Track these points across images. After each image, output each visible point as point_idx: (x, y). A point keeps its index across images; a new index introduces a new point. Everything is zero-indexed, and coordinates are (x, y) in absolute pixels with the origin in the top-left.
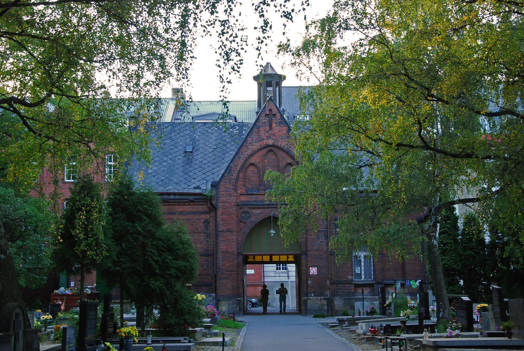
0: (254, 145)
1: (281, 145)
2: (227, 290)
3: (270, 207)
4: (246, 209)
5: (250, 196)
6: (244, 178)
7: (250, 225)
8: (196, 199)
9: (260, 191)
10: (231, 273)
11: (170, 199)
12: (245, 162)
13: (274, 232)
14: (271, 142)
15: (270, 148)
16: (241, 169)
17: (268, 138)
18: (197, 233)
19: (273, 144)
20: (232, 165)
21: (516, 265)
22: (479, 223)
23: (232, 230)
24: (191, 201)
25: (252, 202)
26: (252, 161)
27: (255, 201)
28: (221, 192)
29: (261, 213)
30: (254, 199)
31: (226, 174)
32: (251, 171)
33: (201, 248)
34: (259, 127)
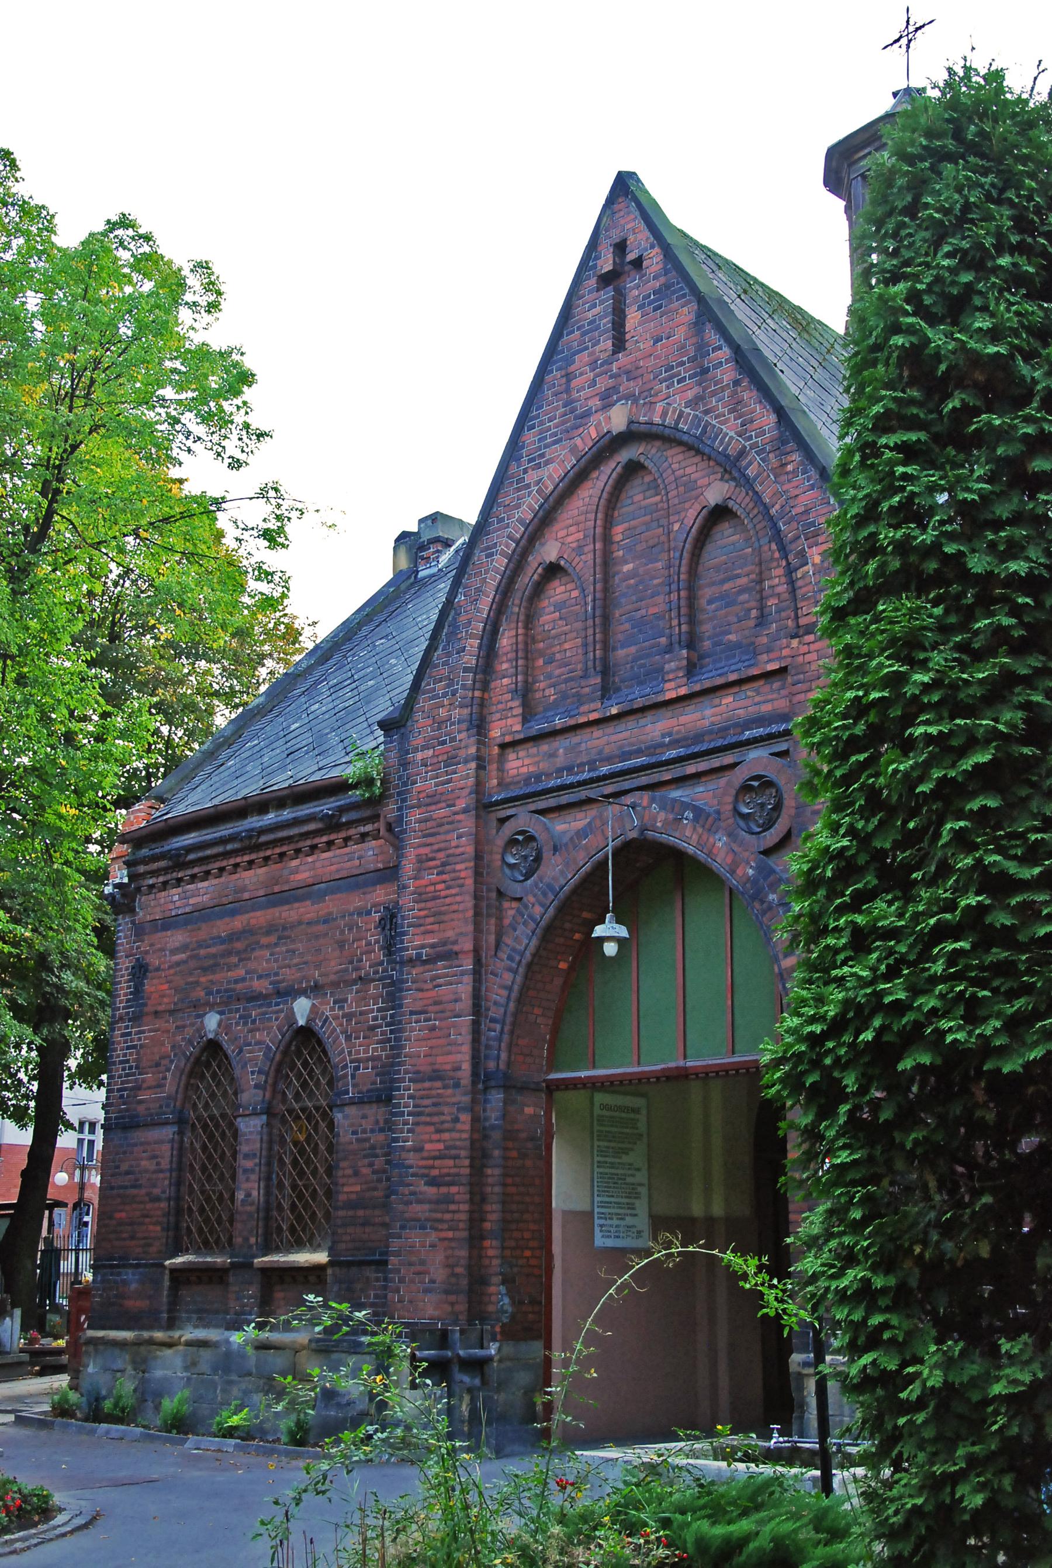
0: (547, 463)
1: (664, 414)
2: (426, 1291)
3: (626, 785)
4: (523, 819)
5: (545, 747)
6: (527, 651)
7: (538, 910)
8: (342, 810)
9: (584, 708)
10: (444, 1190)
11: (262, 831)
12: (518, 562)
13: (622, 932)
14: (618, 419)
15: (625, 455)
16: (500, 608)
17: (608, 399)
18: (354, 982)
19: (631, 422)
20: (460, 598)
21: (943, 1254)
22: (1033, 222)
23: (456, 948)
24: (332, 824)
25: (559, 771)
26: (550, 551)
27: (570, 769)
28: (416, 750)
29: (582, 834)
30: (560, 761)
31: (439, 652)
32: (558, 607)
33: (368, 1059)
34: (569, 360)
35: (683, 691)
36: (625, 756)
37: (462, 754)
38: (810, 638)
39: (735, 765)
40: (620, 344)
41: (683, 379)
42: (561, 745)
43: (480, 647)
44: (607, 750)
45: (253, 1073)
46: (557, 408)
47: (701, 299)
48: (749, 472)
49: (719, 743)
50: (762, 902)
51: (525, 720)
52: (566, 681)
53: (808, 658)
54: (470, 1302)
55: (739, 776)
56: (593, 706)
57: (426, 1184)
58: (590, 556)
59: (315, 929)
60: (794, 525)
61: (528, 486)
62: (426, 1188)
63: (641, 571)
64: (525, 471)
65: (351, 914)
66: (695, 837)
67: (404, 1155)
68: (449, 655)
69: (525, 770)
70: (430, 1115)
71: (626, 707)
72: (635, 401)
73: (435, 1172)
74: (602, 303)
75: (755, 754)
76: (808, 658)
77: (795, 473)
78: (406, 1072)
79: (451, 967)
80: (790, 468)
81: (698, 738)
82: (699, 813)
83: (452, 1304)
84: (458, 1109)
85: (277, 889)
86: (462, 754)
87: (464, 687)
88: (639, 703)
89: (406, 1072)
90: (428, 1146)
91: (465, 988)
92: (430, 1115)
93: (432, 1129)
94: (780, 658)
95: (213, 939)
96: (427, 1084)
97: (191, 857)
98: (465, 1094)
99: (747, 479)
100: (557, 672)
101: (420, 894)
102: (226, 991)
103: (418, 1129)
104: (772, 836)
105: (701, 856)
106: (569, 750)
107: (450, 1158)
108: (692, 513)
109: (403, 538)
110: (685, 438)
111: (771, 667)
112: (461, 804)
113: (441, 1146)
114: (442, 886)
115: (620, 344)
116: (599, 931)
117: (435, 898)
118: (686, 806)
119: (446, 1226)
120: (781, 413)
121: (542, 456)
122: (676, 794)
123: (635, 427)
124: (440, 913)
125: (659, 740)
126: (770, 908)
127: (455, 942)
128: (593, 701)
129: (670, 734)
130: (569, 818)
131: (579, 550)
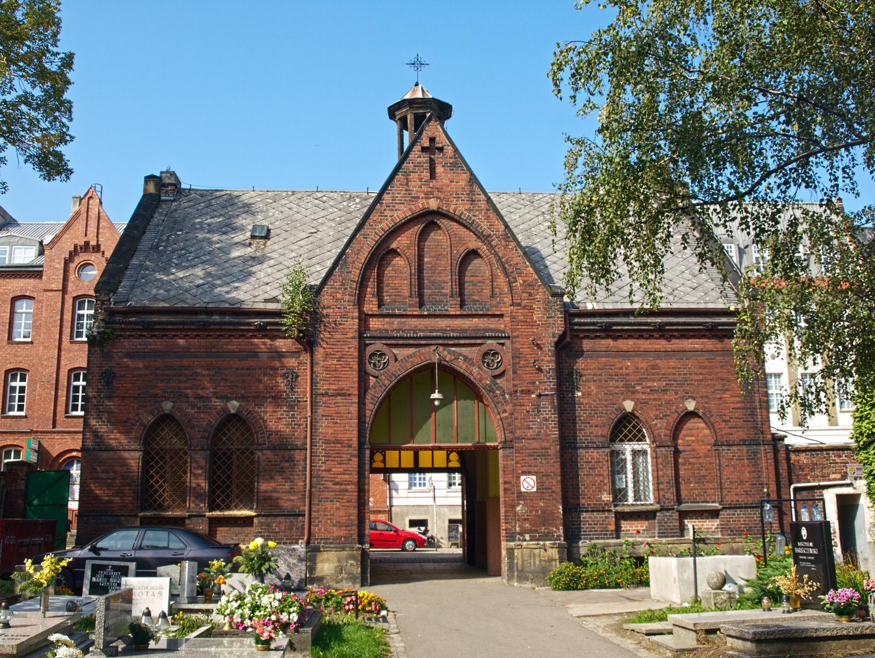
0: (396, 210)
7: (387, 382)
15: (430, 218)
17: (428, 196)
19: (439, 208)
30: (395, 326)
35: (458, 313)
36: (431, 331)
37: (350, 314)
38: (519, 307)
39: (482, 344)
40: (433, 176)
41: (464, 200)
42: (396, 321)
43: (360, 273)
44: (419, 327)
45: (199, 431)
46: (402, 190)
47: (472, 174)
48: (493, 243)
49: (475, 335)
50: (494, 393)
51: (379, 306)
52: (396, 295)
53: (517, 314)
54: (359, 530)
55: (484, 349)
56: (415, 309)
57: (333, 484)
58: (413, 251)
59: (755, 443)
60: (511, 267)
61: (386, 216)
62: (333, 486)
63: (433, 262)
64: (385, 210)
65: (267, 368)
66: (464, 366)
67: (320, 472)
68: (342, 273)
69: (377, 326)
70: (334, 457)
71: (431, 312)
72: (441, 200)
73: (337, 480)
74: (424, 157)
75: (490, 342)
76: (517, 314)
77: (512, 249)
78: (320, 439)
79: (346, 399)
80: (510, 247)
81: (465, 331)
82: (466, 358)
83: (349, 531)
84: (351, 456)
85: (213, 350)
86: (350, 314)
87: (351, 288)
88: (438, 313)
89: (320, 439)
90: (333, 470)
91: (354, 409)
92: (334, 457)
93: (336, 463)
94: (500, 311)
95: (165, 367)
96: (332, 445)
97: (157, 327)
98: (355, 450)
99: (492, 246)
100: (391, 291)
101: (327, 368)
102: (177, 392)
103: (327, 463)
104: (498, 372)
105: (467, 374)
106: (399, 323)
107: (348, 474)
108: (462, 249)
109: (149, 178)
110: (464, 222)
111: (497, 313)
112: (350, 335)
113: (342, 470)
114: (340, 366)
115: (433, 176)
116: (433, 396)
117: (336, 371)
118: (460, 354)
119: (344, 501)
120: (507, 227)
121: (394, 206)
122: (453, 349)
123: (440, 210)
124: (338, 377)
125: (445, 328)
126: (497, 396)
127: (348, 390)
128: (415, 307)
129: (449, 327)
130: (399, 349)
131: (408, 247)
